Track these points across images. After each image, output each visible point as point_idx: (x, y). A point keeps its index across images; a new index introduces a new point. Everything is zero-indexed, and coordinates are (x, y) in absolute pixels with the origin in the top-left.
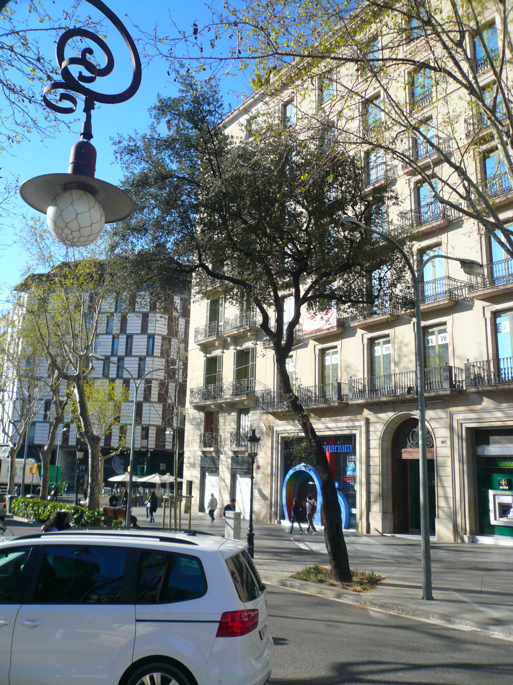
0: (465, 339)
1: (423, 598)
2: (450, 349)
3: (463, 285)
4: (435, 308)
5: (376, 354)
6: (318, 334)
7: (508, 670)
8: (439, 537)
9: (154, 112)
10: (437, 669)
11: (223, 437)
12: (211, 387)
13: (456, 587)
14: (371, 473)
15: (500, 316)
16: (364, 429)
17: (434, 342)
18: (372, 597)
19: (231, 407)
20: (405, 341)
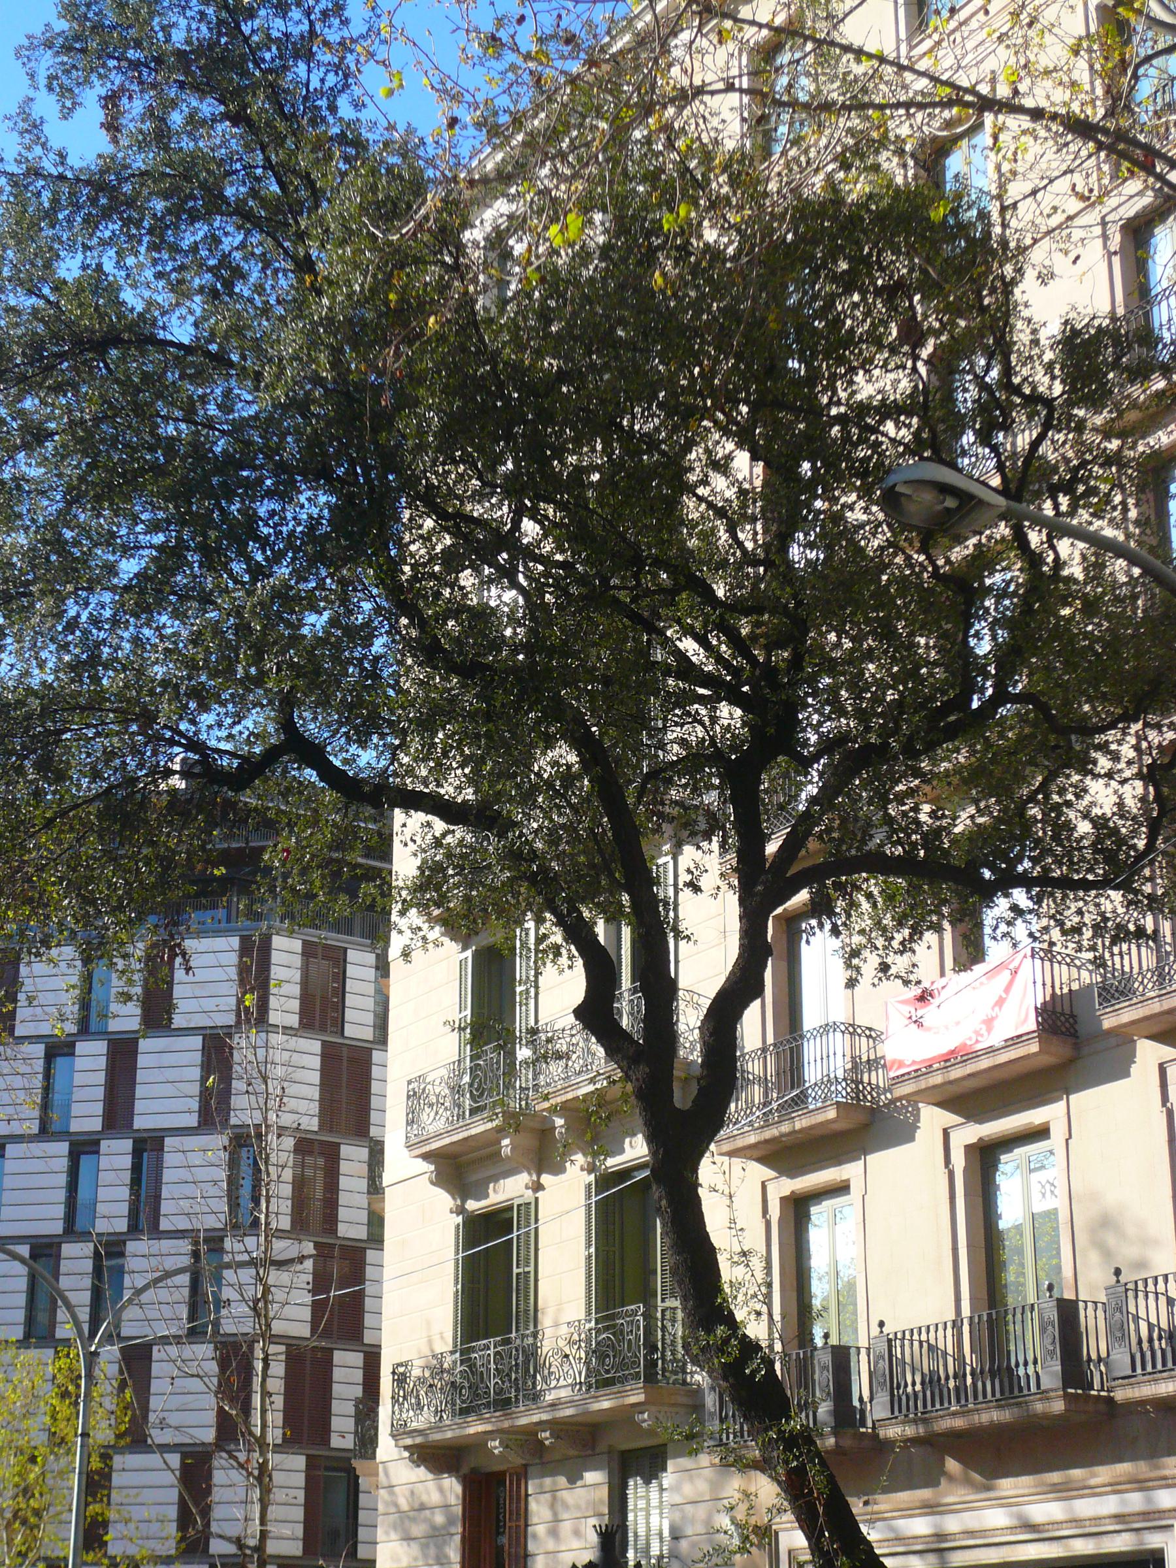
6: (956, 1073)
9: (47, 62)
12: (487, 1350)
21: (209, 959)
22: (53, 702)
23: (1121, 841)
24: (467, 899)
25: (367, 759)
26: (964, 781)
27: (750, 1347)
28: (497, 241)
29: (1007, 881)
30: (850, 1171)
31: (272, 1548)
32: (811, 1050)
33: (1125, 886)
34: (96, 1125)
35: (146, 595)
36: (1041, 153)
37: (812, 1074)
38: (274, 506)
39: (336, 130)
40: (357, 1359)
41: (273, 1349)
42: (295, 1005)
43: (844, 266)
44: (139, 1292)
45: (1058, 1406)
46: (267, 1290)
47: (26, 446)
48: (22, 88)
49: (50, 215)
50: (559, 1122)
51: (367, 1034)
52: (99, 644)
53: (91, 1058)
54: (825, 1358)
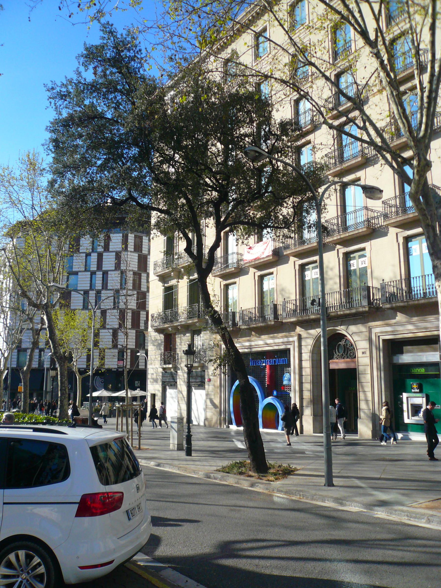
0: (381, 262)
1: (325, 485)
2: (369, 271)
3: (379, 214)
4: (355, 236)
5: (307, 278)
6: (257, 262)
7: (376, 544)
8: (361, 435)
10: (312, 545)
11: (179, 355)
12: (169, 312)
13: (359, 476)
14: (304, 381)
15: (411, 241)
16: (296, 344)
17: (355, 265)
18: (280, 485)
19: (186, 328)
20: (331, 265)
21: (115, 238)
22: (84, 188)
23: (288, 220)
24: (164, 228)
25: (146, 201)
26: (259, 207)
27: (216, 312)
28: (172, 99)
29: (267, 227)
30: (236, 280)
31: (128, 347)
32: (230, 257)
33: (288, 228)
34: (95, 269)
35: (102, 168)
36: (277, 86)
37: (230, 261)
38: (127, 151)
39: (139, 76)
40: (145, 313)
41: (128, 311)
42: (133, 247)
43: (239, 107)
44: (103, 300)
45: (273, 323)
46: (127, 300)
47: (78, 138)
48: (77, 65)
49: (83, 92)
50: (182, 270)
51: (147, 253)
52: (93, 177)
53: (94, 256)
54: (231, 314)
